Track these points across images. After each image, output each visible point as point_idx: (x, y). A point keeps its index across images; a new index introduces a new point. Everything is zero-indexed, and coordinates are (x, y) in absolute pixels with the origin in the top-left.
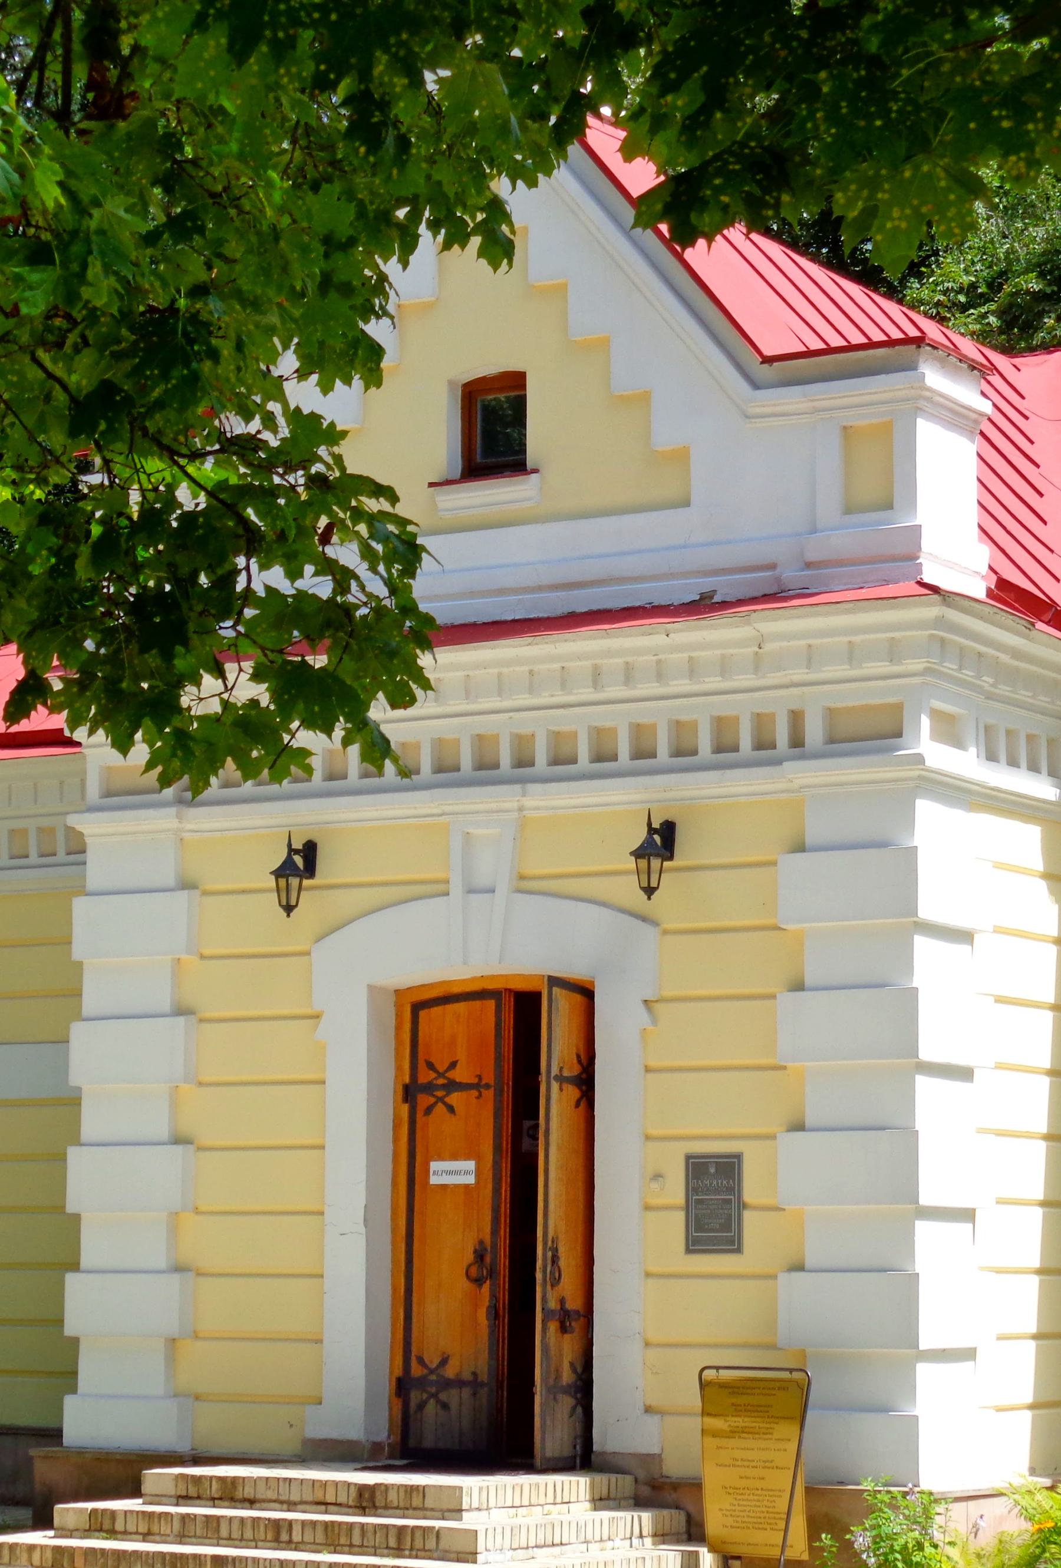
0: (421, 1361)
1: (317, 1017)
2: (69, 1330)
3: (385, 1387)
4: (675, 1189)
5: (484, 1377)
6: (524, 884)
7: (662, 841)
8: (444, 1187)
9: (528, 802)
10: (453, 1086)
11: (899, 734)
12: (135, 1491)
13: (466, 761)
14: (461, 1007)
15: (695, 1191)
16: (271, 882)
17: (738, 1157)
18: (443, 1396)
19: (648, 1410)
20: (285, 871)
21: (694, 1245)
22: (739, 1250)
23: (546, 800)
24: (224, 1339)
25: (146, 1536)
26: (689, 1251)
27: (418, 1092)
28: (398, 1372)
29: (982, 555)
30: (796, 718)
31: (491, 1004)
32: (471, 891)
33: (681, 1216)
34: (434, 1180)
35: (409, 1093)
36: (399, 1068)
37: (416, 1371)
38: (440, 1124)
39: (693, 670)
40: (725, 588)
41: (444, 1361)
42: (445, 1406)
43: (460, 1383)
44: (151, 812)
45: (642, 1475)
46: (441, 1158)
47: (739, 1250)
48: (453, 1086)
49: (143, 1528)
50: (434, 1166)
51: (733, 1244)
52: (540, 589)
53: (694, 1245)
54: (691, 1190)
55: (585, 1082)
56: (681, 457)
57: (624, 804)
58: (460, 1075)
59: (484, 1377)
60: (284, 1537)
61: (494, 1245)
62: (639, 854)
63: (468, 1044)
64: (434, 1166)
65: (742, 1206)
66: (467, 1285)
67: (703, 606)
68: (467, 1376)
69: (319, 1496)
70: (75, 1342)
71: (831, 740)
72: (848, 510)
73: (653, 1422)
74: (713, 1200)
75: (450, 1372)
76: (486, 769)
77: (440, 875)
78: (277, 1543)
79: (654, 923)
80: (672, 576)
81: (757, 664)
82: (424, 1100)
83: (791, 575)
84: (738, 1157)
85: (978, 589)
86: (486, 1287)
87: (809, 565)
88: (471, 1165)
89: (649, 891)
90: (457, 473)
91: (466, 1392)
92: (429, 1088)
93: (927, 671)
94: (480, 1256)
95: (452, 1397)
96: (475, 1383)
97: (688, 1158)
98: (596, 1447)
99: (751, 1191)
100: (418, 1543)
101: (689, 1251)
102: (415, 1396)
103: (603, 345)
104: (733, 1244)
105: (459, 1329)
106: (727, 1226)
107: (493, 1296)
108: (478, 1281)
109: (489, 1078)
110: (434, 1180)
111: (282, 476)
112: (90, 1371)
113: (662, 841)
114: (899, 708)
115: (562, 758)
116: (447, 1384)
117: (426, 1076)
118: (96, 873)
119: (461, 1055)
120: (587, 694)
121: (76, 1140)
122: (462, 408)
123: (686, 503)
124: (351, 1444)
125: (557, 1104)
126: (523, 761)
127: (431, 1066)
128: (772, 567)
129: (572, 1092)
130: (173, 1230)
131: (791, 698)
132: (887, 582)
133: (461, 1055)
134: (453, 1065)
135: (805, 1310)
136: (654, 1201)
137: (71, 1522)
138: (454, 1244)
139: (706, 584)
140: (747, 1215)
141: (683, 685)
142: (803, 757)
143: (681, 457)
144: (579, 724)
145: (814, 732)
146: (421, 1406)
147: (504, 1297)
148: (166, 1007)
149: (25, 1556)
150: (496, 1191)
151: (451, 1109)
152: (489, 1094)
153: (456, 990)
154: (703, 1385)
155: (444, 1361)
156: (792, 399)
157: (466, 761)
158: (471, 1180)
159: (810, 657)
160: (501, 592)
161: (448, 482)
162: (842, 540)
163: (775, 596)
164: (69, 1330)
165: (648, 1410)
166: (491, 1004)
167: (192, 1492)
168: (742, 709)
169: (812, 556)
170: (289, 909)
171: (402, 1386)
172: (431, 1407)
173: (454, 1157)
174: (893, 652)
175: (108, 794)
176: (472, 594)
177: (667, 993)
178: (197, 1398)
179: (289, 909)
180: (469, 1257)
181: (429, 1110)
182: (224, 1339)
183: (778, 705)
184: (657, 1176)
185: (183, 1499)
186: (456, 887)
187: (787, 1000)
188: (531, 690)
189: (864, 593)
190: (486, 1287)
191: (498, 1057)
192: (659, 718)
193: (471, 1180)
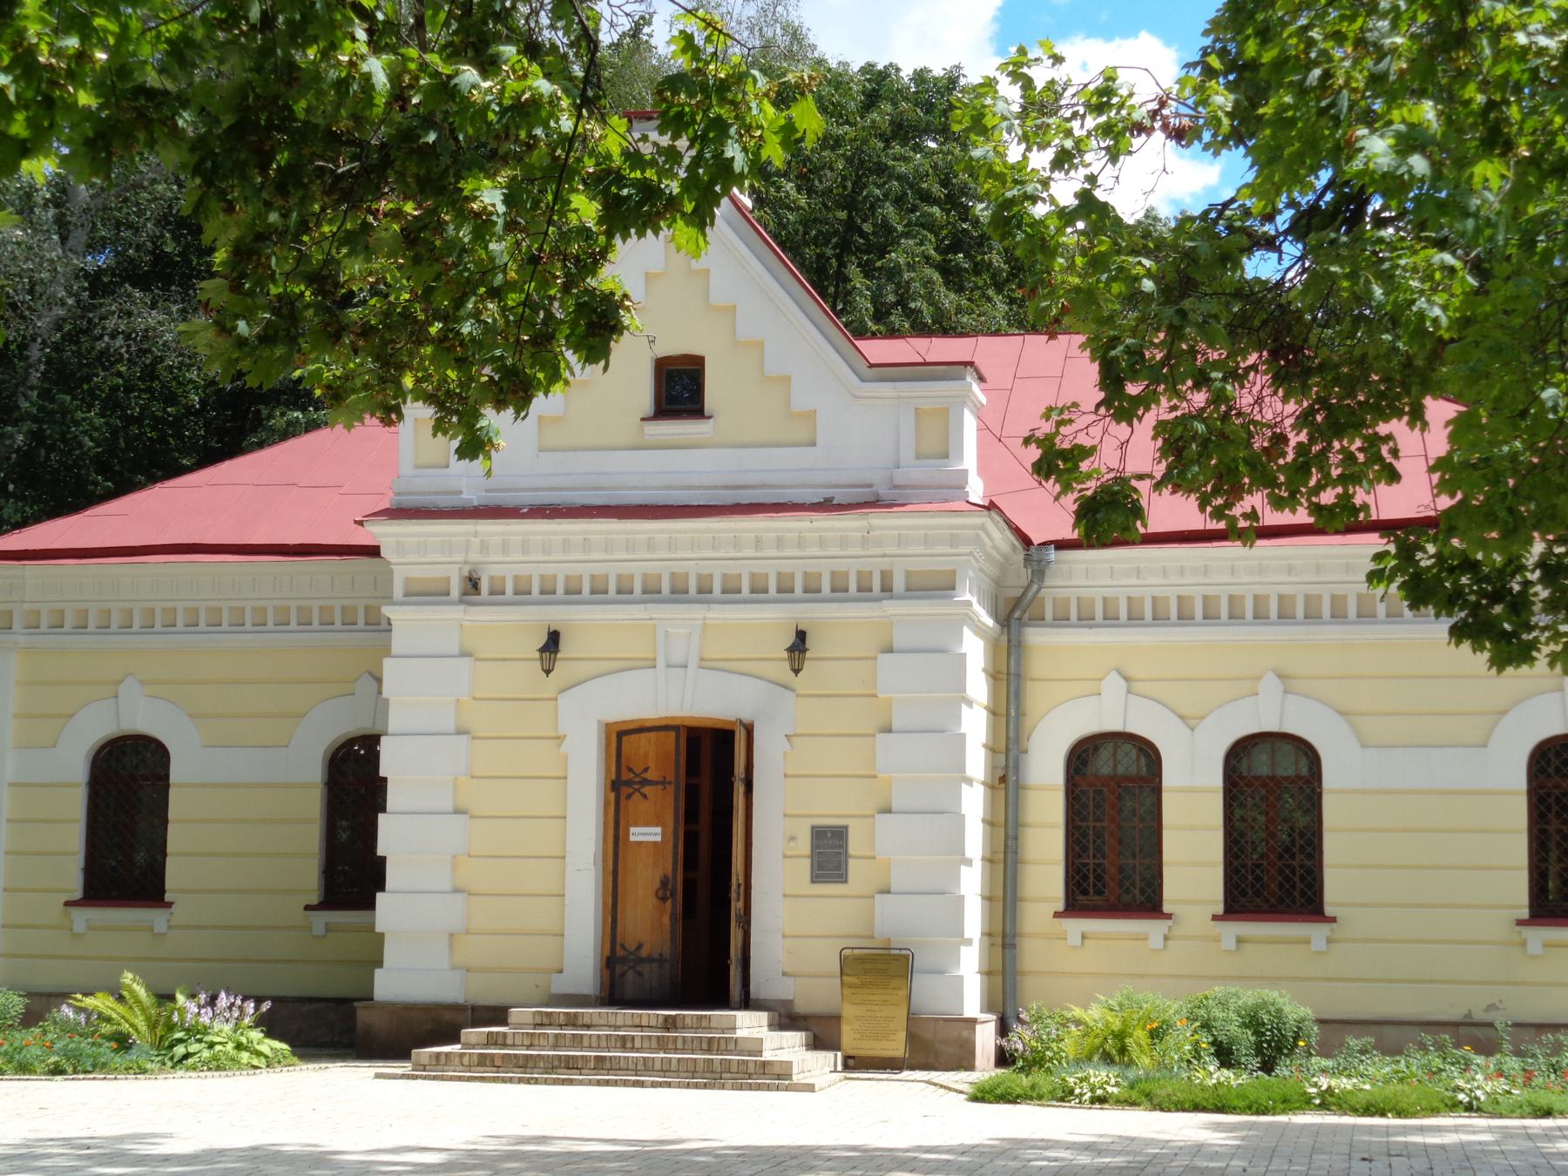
0: (623, 946)
1: (560, 739)
2: (378, 929)
4: (804, 845)
5: (667, 955)
6: (705, 664)
7: (800, 644)
8: (640, 843)
9: (709, 615)
10: (645, 782)
11: (954, 589)
12: (504, 1023)
13: (666, 587)
14: (652, 735)
15: (818, 847)
16: (537, 655)
17: (846, 827)
18: (639, 968)
19: (784, 974)
21: (816, 878)
22: (846, 882)
23: (720, 614)
25: (529, 1047)
26: (813, 882)
27: (622, 785)
28: (607, 953)
30: (886, 576)
31: (673, 734)
32: (668, 666)
33: (808, 861)
34: (632, 838)
36: (608, 770)
38: (636, 804)
39: (822, 543)
41: (640, 947)
42: (640, 974)
43: (650, 960)
44: (446, 608)
45: (783, 1011)
46: (637, 825)
47: (846, 882)
48: (645, 782)
49: (527, 1042)
50: (632, 830)
51: (842, 878)
52: (716, 487)
53: (816, 878)
54: (814, 846)
56: (811, 416)
57: (776, 619)
58: (650, 775)
59: (667, 955)
60: (629, 1045)
61: (674, 877)
62: (542, 650)
63: (654, 757)
64: (632, 830)
65: (847, 856)
66: (655, 900)
67: (826, 506)
68: (655, 955)
69: (637, 1022)
70: (382, 935)
71: (908, 589)
72: (918, 457)
73: (790, 981)
74: (829, 853)
75: (644, 953)
76: (679, 593)
77: (650, 655)
78: (624, 1047)
79: (793, 690)
80: (804, 486)
81: (864, 542)
82: (625, 790)
83: (884, 492)
84: (846, 827)
86: (669, 903)
87: (895, 487)
88: (658, 830)
89: (797, 671)
91: (654, 965)
92: (629, 783)
93: (971, 554)
94: (664, 883)
95: (646, 969)
96: (661, 960)
97: (813, 828)
98: (752, 996)
99: (853, 848)
100: (723, 1046)
101: (813, 882)
102: (619, 969)
103: (760, 345)
104: (842, 878)
105: (651, 924)
106: (838, 867)
107: (674, 907)
108: (664, 899)
109: (671, 777)
110: (632, 838)
112: (390, 953)
113: (800, 644)
114: (954, 572)
115: (839, 588)
116: (641, 960)
117: (625, 776)
118: (398, 642)
119: (652, 764)
120: (751, 553)
121: (384, 810)
123: (814, 444)
126: (887, 589)
127: (630, 770)
128: (870, 486)
130: (454, 866)
131: (884, 564)
132: (946, 501)
133: (652, 764)
134: (646, 770)
135: (894, 919)
136: (789, 853)
137: (473, 1040)
138: (644, 881)
139: (829, 493)
140: (851, 862)
141: (815, 551)
142: (891, 598)
143: (811, 416)
144: (744, 570)
145: (899, 584)
146: (623, 974)
147: (680, 909)
148: (452, 729)
149: (457, 1060)
150: (675, 846)
151: (645, 796)
152: (671, 788)
153: (648, 724)
155: (640, 947)
156: (887, 389)
157: (666, 587)
158: (659, 839)
159: (900, 541)
160: (689, 488)
162: (916, 473)
163: (874, 503)
164: (378, 929)
165: (784, 974)
166: (673, 734)
167: (546, 1021)
168: (852, 567)
169: (897, 481)
170: (548, 672)
172: (630, 974)
173: (647, 824)
174: (953, 541)
175: (406, 595)
176: (669, 488)
177: (799, 731)
178: (468, 970)
179: (548, 672)
180: (657, 884)
181: (629, 797)
183: (875, 566)
184: (793, 838)
185: (487, 1045)
186: (661, 663)
187: (881, 737)
188: (713, 548)
189: (935, 506)
190: (669, 903)
191: (677, 765)
192: (797, 569)
193: (659, 839)
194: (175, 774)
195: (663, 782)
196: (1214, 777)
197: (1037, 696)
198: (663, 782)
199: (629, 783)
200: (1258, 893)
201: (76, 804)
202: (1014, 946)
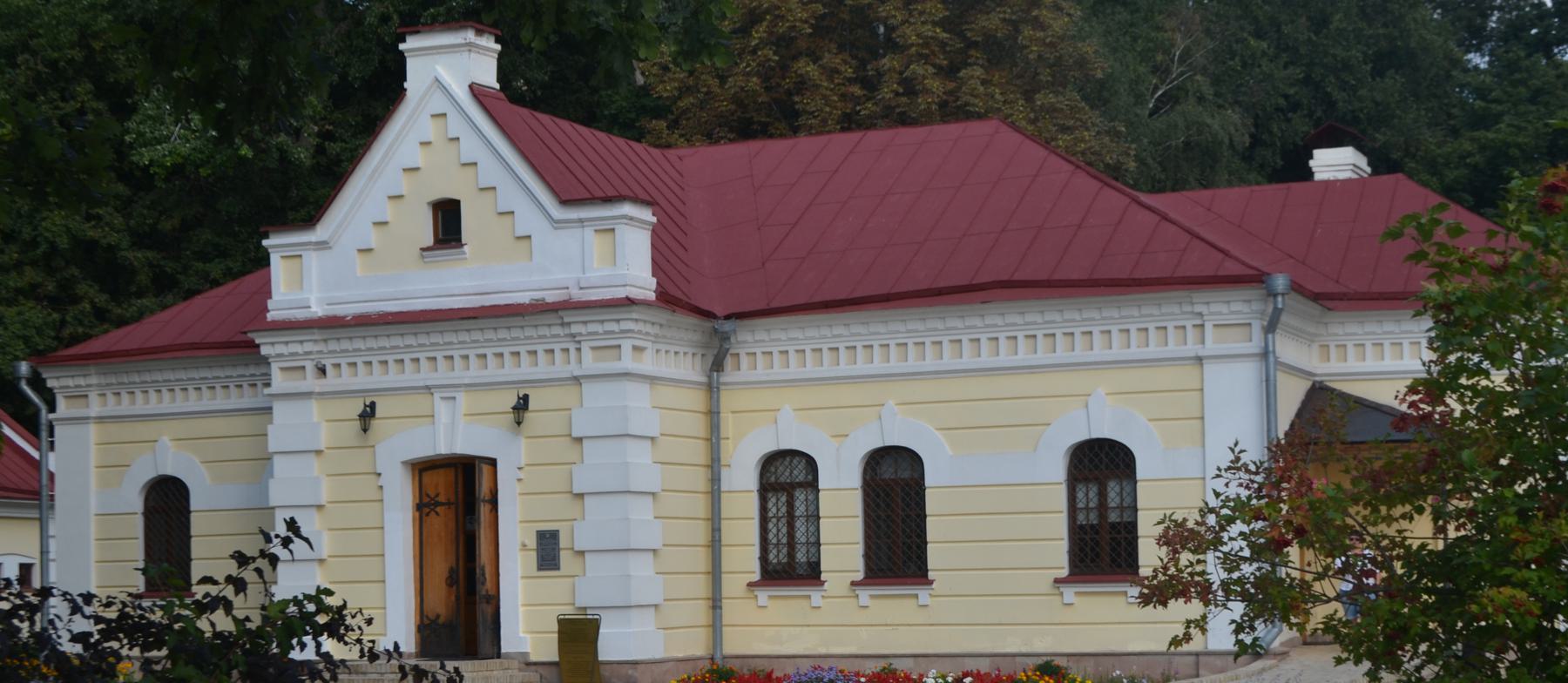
4: (532, 542)
27: (424, 507)
29: (652, 283)
55: (494, 502)
58: (442, 499)
75: (441, 620)
85: (652, 296)
92: (427, 505)
125: (484, 510)
133: (442, 490)
147: (479, 587)
155: (438, 616)
180: (446, 575)
194: (194, 504)
195: (448, 504)
198: (448, 504)
199: (427, 505)
200: (1093, 561)
201: (137, 525)
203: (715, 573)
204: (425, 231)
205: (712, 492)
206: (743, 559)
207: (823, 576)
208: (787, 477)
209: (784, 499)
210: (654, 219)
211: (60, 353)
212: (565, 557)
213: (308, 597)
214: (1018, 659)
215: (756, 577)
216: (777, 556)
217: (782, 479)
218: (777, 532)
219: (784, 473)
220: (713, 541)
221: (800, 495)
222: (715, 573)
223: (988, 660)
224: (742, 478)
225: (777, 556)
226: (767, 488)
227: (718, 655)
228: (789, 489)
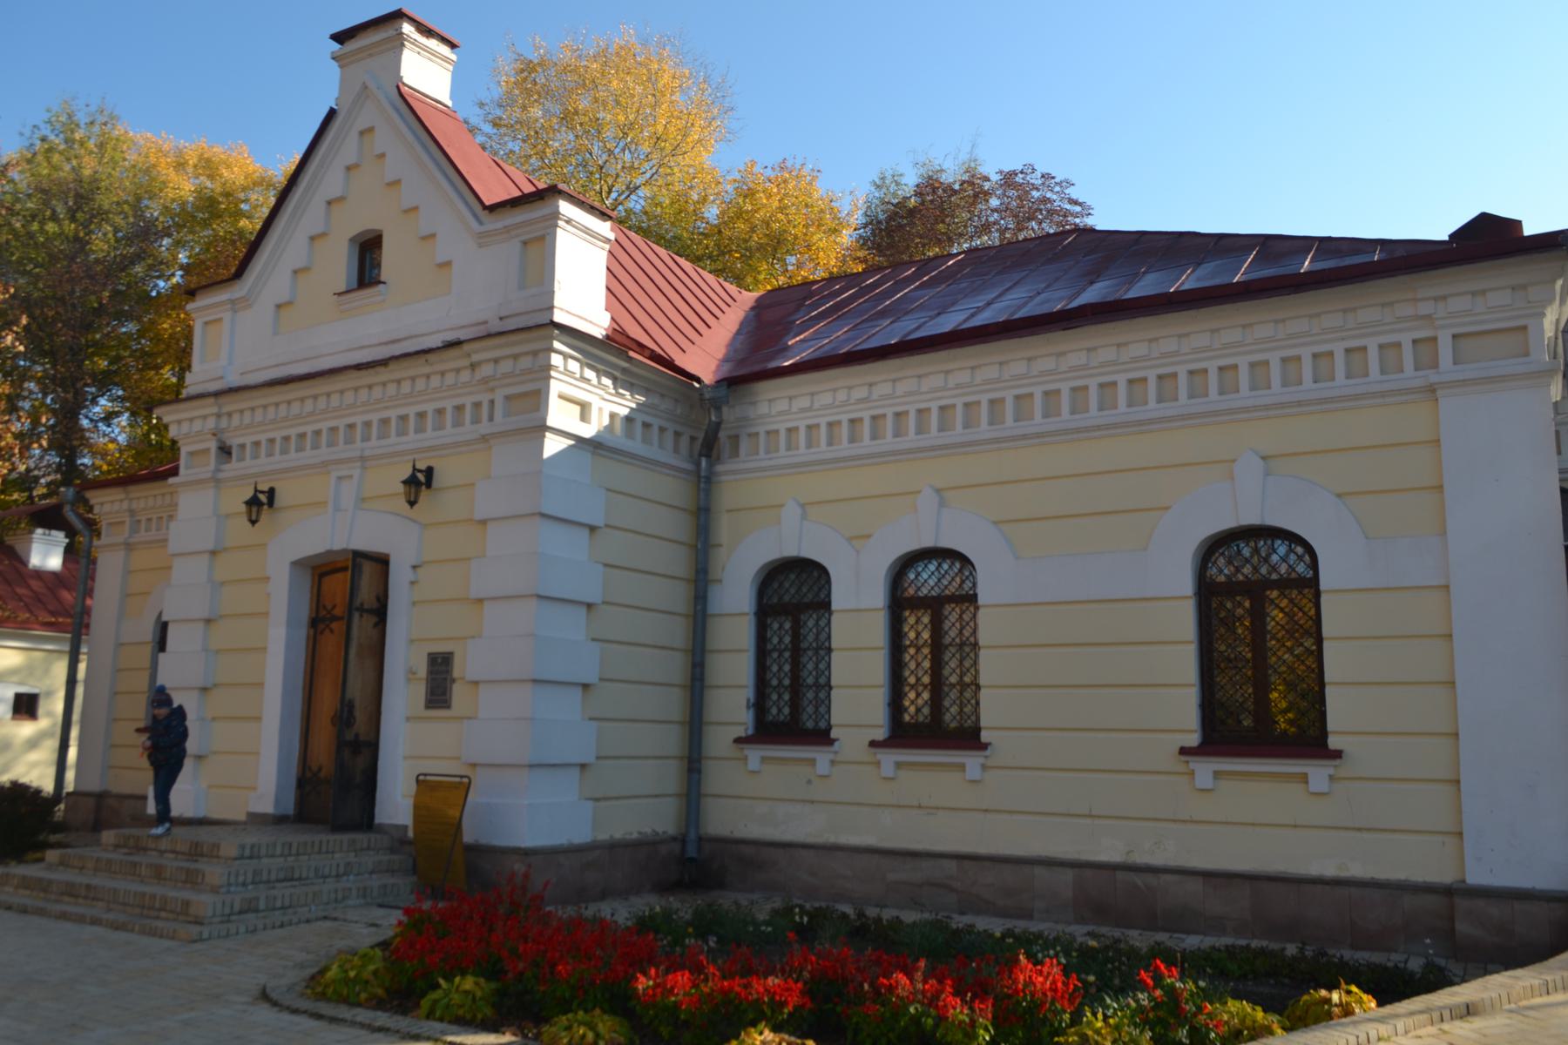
3: (293, 782)
4: (422, 670)
20: (253, 503)
24: (1347, 829)
35: (314, 623)
37: (308, 775)
40: (462, 335)
41: (320, 769)
74: (440, 680)
75: (322, 774)
82: (321, 626)
84: (451, 654)
90: (355, 285)
106: (444, 693)
111: (12, 254)
122: (961, 347)
124: (264, 816)
128: (486, 322)
129: (371, 620)
134: (334, 607)
154: (418, 781)
155: (320, 769)
161: (348, 292)
171: (301, 783)
182: (1347, 829)
196: (877, 596)
197: (724, 528)
202: (699, 771)
203: (695, 723)
204: (391, 259)
205: (695, 616)
206: (732, 703)
207: (833, 734)
208: (794, 591)
209: (787, 625)
210: (612, 236)
211: (631, 354)
212: (458, 692)
213: (976, 677)
214: (1120, 875)
215: (881, 734)
216: (779, 710)
217: (787, 598)
218: (918, 666)
219: (927, 579)
220: (693, 679)
221: (952, 614)
222: (695, 723)
223: (1069, 875)
224: (736, 596)
225: (916, 703)
226: (899, 603)
227: (692, 835)
228: (795, 611)
